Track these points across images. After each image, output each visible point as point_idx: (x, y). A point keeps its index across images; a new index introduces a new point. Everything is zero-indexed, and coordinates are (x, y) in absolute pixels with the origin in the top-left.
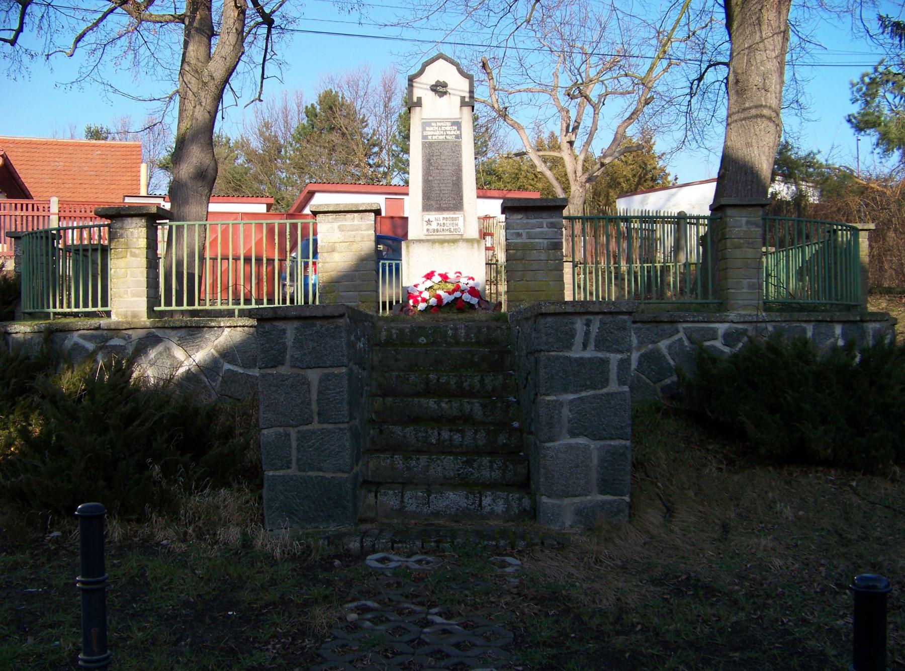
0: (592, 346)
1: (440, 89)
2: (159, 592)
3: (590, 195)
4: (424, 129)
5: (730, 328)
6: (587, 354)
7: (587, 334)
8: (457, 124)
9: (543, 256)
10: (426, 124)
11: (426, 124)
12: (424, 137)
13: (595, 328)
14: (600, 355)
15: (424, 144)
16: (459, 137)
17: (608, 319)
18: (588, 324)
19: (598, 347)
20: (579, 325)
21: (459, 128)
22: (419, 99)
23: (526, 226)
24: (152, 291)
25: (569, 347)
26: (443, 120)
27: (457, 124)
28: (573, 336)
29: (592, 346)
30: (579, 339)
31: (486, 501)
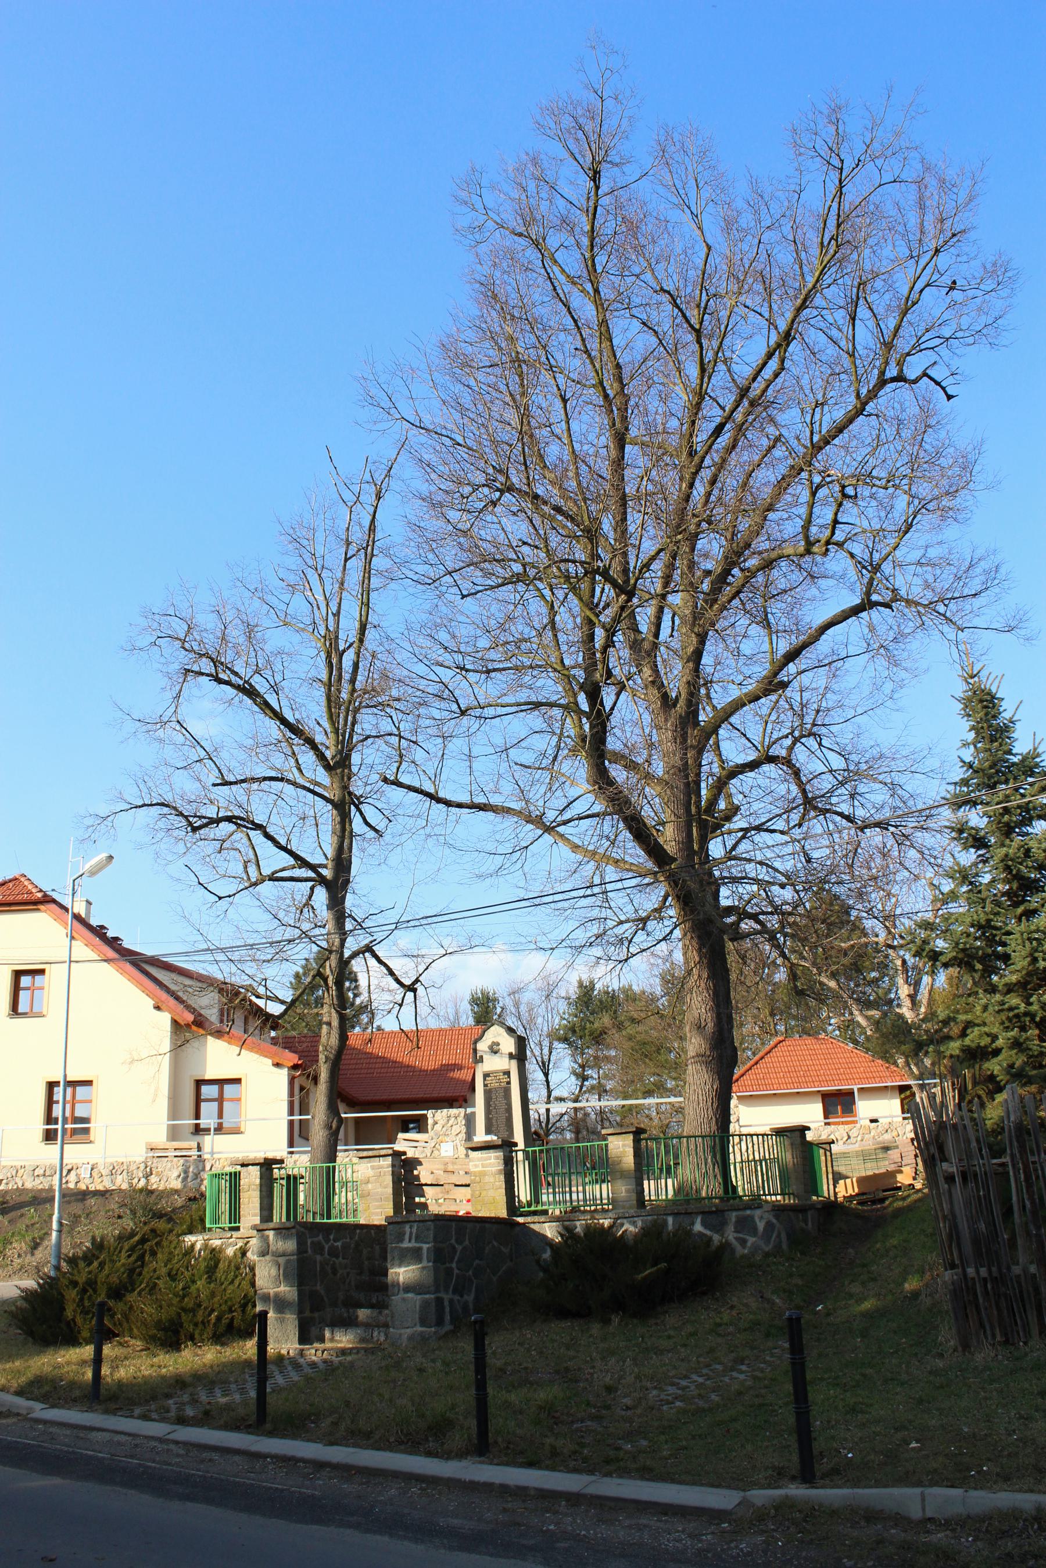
0: (413, 1240)
1: (494, 1050)
2: (17, 1261)
3: (164, 1205)
4: (485, 1080)
5: (655, 1221)
6: (410, 1245)
7: (411, 1233)
8: (507, 1073)
9: (492, 1180)
10: (486, 1075)
11: (486, 1075)
12: (485, 1085)
13: (414, 1230)
14: (417, 1245)
15: (485, 1091)
16: (509, 1083)
17: (421, 1224)
18: (411, 1227)
19: (416, 1241)
20: (407, 1228)
21: (509, 1077)
22: (481, 1057)
23: (481, 1159)
24: (266, 1213)
25: (402, 1241)
26: (496, 1072)
27: (507, 1073)
28: (404, 1234)
29: (413, 1240)
30: (407, 1236)
31: (375, 1334)
